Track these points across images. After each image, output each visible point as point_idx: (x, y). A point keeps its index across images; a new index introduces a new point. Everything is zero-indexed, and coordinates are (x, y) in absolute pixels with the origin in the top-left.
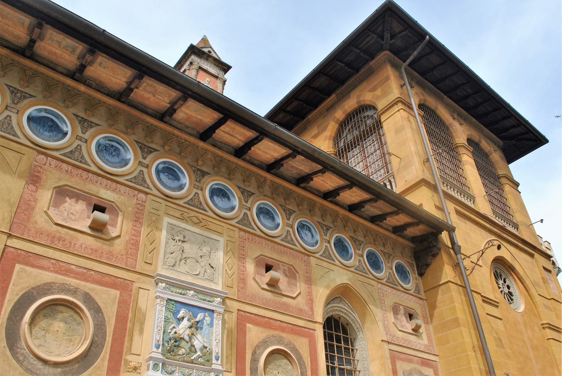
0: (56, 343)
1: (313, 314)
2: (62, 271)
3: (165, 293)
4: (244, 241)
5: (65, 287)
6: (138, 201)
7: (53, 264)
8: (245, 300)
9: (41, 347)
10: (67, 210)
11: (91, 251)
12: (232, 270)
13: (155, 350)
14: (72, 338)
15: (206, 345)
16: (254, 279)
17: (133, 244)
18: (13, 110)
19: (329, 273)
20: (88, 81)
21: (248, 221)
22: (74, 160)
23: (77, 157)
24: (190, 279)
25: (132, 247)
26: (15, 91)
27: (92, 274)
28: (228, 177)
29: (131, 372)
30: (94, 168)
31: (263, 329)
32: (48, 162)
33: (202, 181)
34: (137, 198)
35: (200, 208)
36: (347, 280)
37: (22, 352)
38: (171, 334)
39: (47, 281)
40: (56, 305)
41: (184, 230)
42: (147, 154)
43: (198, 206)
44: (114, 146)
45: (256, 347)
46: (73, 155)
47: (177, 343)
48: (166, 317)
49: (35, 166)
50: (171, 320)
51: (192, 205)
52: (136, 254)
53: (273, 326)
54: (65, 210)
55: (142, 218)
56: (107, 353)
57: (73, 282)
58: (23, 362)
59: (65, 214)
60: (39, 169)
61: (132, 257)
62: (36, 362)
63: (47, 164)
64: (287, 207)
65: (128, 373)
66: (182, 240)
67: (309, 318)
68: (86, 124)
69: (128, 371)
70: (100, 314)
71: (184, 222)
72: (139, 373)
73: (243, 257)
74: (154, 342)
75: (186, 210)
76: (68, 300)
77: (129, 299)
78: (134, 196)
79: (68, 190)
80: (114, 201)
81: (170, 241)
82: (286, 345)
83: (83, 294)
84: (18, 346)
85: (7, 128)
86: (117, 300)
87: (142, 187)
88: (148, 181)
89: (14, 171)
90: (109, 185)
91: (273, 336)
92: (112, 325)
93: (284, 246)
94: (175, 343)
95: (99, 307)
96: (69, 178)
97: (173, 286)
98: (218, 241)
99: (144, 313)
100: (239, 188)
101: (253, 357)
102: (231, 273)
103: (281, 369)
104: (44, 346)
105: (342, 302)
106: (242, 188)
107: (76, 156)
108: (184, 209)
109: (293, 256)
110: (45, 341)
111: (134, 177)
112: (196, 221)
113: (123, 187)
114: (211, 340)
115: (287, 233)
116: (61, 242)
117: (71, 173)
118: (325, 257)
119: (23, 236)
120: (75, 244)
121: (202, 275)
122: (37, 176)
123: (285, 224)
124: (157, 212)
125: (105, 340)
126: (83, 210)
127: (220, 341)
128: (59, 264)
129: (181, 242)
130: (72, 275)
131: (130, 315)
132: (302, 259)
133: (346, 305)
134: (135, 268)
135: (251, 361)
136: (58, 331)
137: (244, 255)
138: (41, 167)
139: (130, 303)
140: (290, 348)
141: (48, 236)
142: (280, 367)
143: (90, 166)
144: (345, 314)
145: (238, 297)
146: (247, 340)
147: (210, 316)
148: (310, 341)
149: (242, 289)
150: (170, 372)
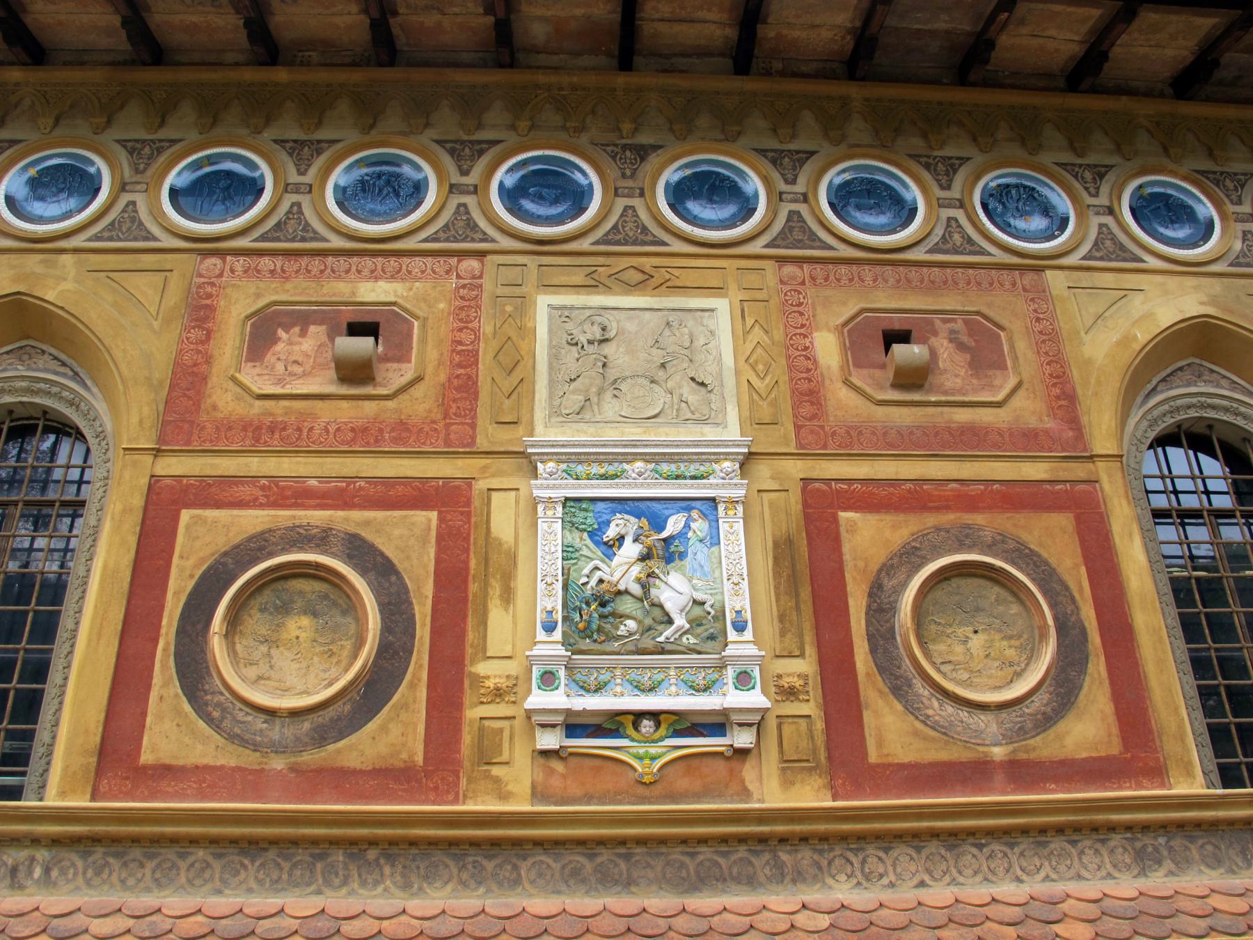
0: (298, 666)
2: (287, 498)
3: (554, 487)
4: (799, 288)
5: (298, 533)
6: (461, 281)
7: (263, 488)
8: (825, 447)
9: (263, 682)
10: (283, 357)
11: (351, 434)
14: (334, 648)
15: (699, 596)
16: (847, 383)
17: (458, 389)
18: (138, 187)
19: (1124, 300)
20: (300, 54)
21: (804, 232)
22: (286, 241)
23: (295, 231)
24: (633, 433)
26: (138, 146)
27: (361, 488)
28: (722, 137)
29: (489, 703)
30: (337, 242)
31: (901, 517)
32: (227, 268)
33: (640, 174)
34: (457, 274)
35: (644, 243)
36: (1202, 303)
37: (216, 700)
38: (589, 587)
39: (254, 531)
40: (286, 578)
41: (602, 312)
42: (472, 161)
44: (384, 174)
45: (880, 571)
46: (281, 231)
47: (608, 609)
48: (568, 547)
49: (199, 287)
51: (618, 243)
52: (471, 410)
53: (933, 502)
54: (279, 359)
56: (421, 666)
57: (316, 517)
58: (221, 722)
59: (280, 367)
60: (209, 289)
62: (250, 718)
63: (225, 274)
64: (936, 153)
66: (598, 337)
67: (1063, 450)
68: (303, 152)
69: (482, 703)
70: (393, 578)
71: (598, 293)
72: (514, 702)
73: (802, 331)
74: (540, 616)
75: (601, 260)
76: (290, 562)
77: (465, 523)
78: (447, 272)
79: (280, 312)
80: (392, 299)
81: (563, 352)
82: (989, 546)
83: (343, 539)
84: (207, 687)
85: (129, 229)
86: (434, 533)
88: (483, 224)
89: (154, 313)
90: (379, 268)
92: (426, 597)
93: (942, 265)
94: (601, 609)
95: (388, 560)
97: (580, 462)
98: (712, 310)
99: (510, 549)
100: (762, 152)
102: (767, 385)
104: (268, 679)
106: (772, 151)
107: (291, 231)
108: (593, 258)
109: (979, 284)
110: (271, 667)
111: (444, 226)
112: (637, 277)
113: (417, 259)
115: (948, 226)
116: (277, 436)
118: (1101, 259)
119: (189, 445)
120: (311, 429)
122: (207, 306)
123: (935, 203)
124: (517, 291)
125: (413, 636)
126: (320, 346)
127: (745, 576)
128: (277, 486)
129: (596, 344)
130: (313, 502)
131: (473, 563)
132: (1014, 284)
133: (1223, 382)
134: (473, 443)
136: (297, 638)
137: (803, 326)
138: (213, 284)
140: (1003, 551)
141: (245, 429)
142: (981, 613)
143: (327, 241)
144: (1226, 410)
145: (800, 445)
146: (847, 557)
147: (704, 515)
148: (1078, 519)
149: (810, 419)
150: (593, 687)
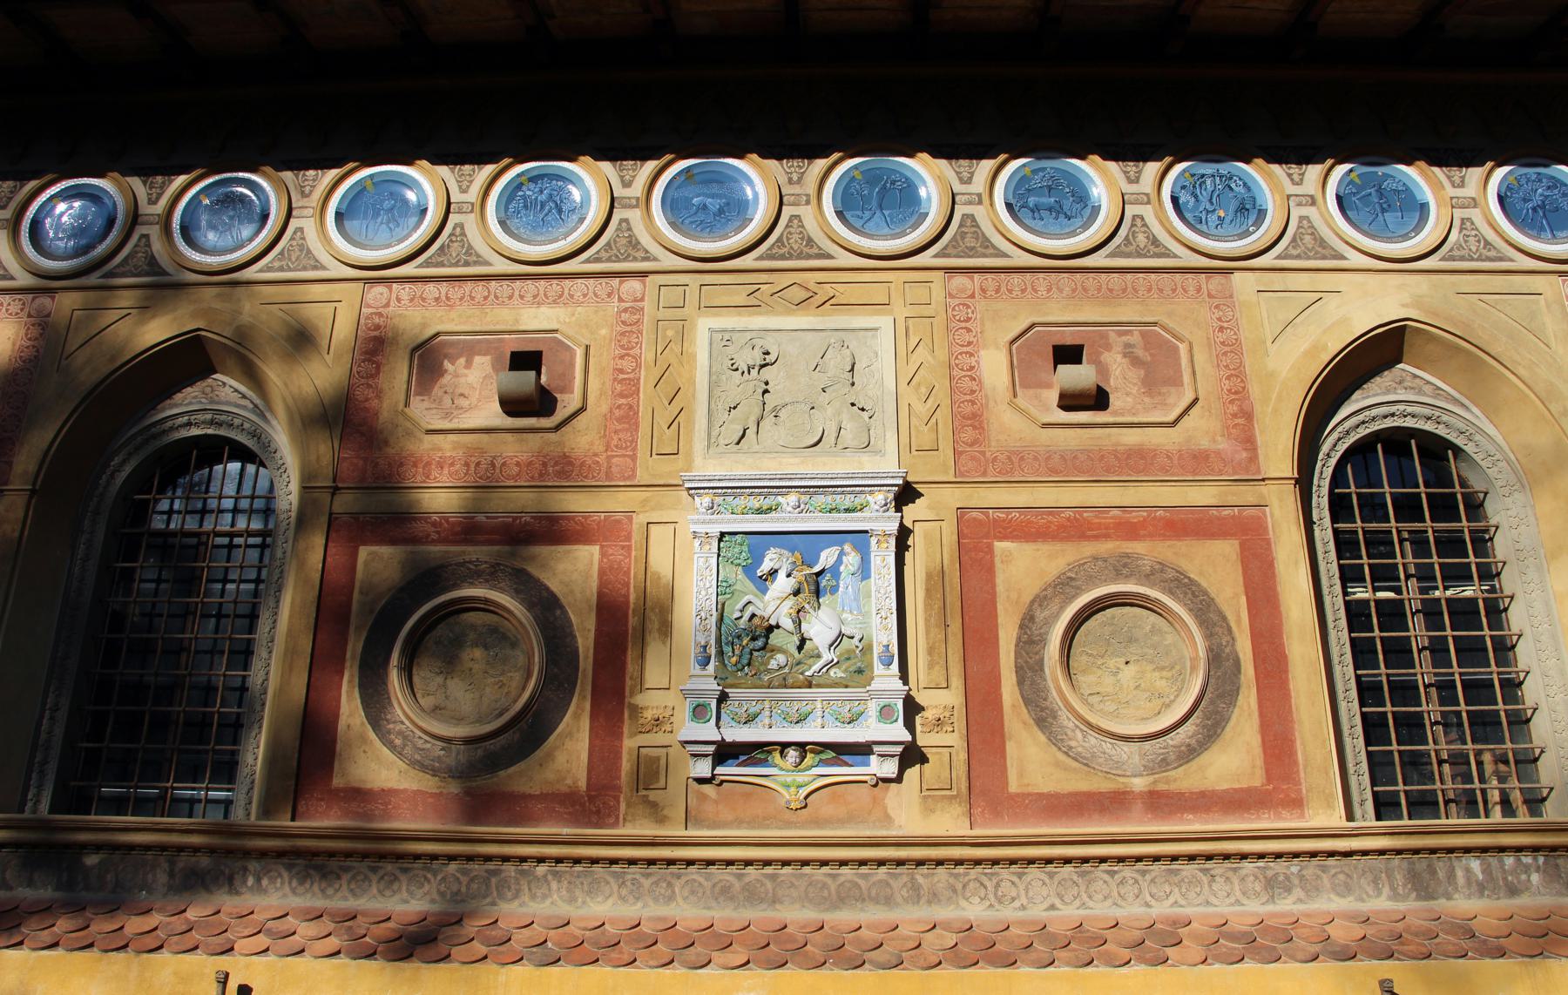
1: (1253, 458)
5: (469, 569)
11: (516, 469)
12: (930, 401)
13: (697, 670)
25: (619, 427)
31: (1058, 546)
37: (397, 728)
42: (634, 170)
43: (801, 252)
45: (1033, 602)
50: (737, 587)
54: (446, 392)
55: (637, 343)
58: (403, 749)
61: (624, 452)
63: (392, 303)
65: (642, 735)
75: (764, 277)
77: (626, 557)
78: (609, 295)
82: (1147, 576)
84: (389, 717)
87: (631, 261)
91: (1096, 559)
96: (444, 313)
101: (1025, 633)
103: (1133, 648)
105: (1406, 384)
107: (454, 255)
114: (866, 615)
116: (446, 471)
117: (448, 298)
121: (829, 439)
135: (1017, 645)
137: (970, 343)
138: (380, 315)
139: (629, 569)
146: (1000, 588)
147: (856, 548)
